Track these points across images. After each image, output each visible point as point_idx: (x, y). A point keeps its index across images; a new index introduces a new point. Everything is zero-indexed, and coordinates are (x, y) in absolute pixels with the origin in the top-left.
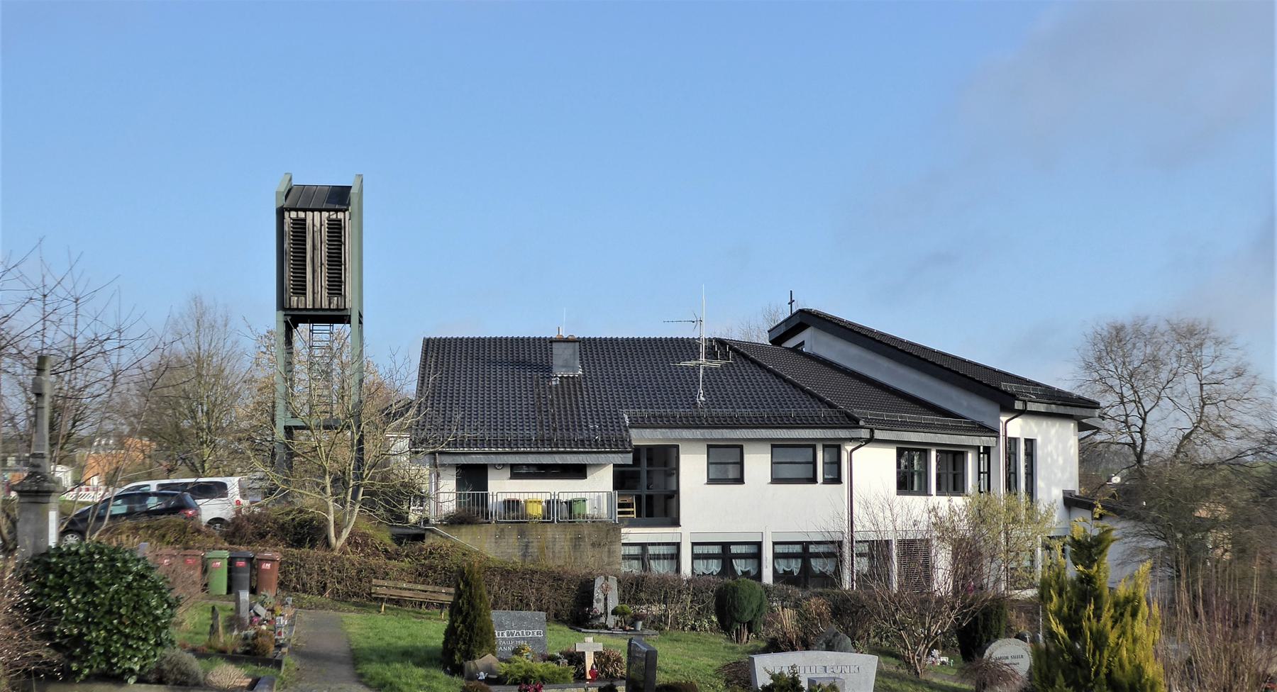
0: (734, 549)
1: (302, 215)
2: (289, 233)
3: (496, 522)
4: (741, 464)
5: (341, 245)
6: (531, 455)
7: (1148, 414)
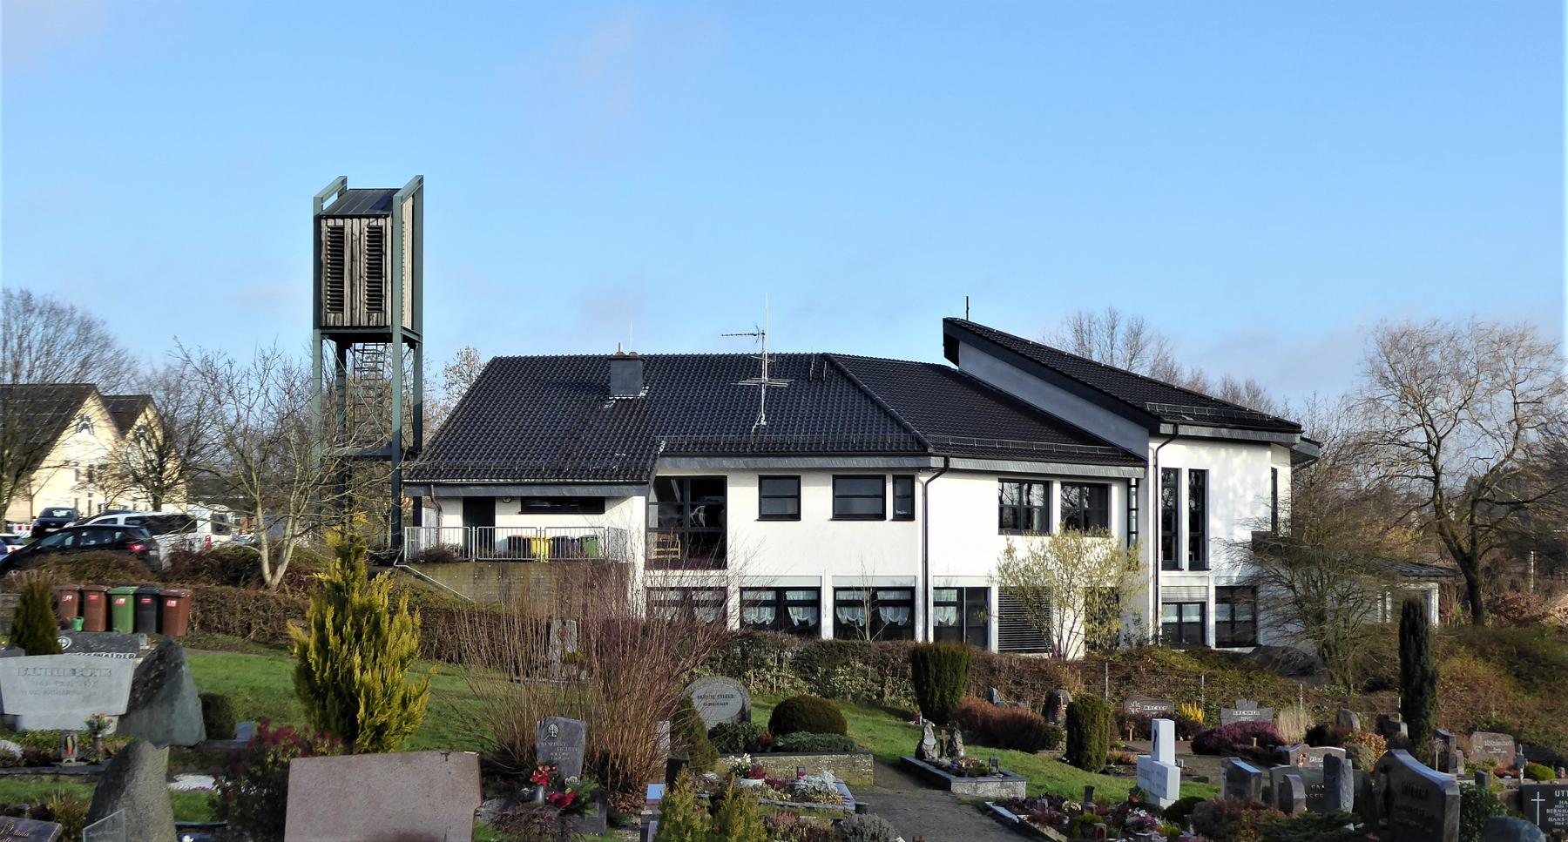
0: (790, 596)
3: (476, 560)
4: (798, 497)
5: (382, 256)
7: (1443, 441)
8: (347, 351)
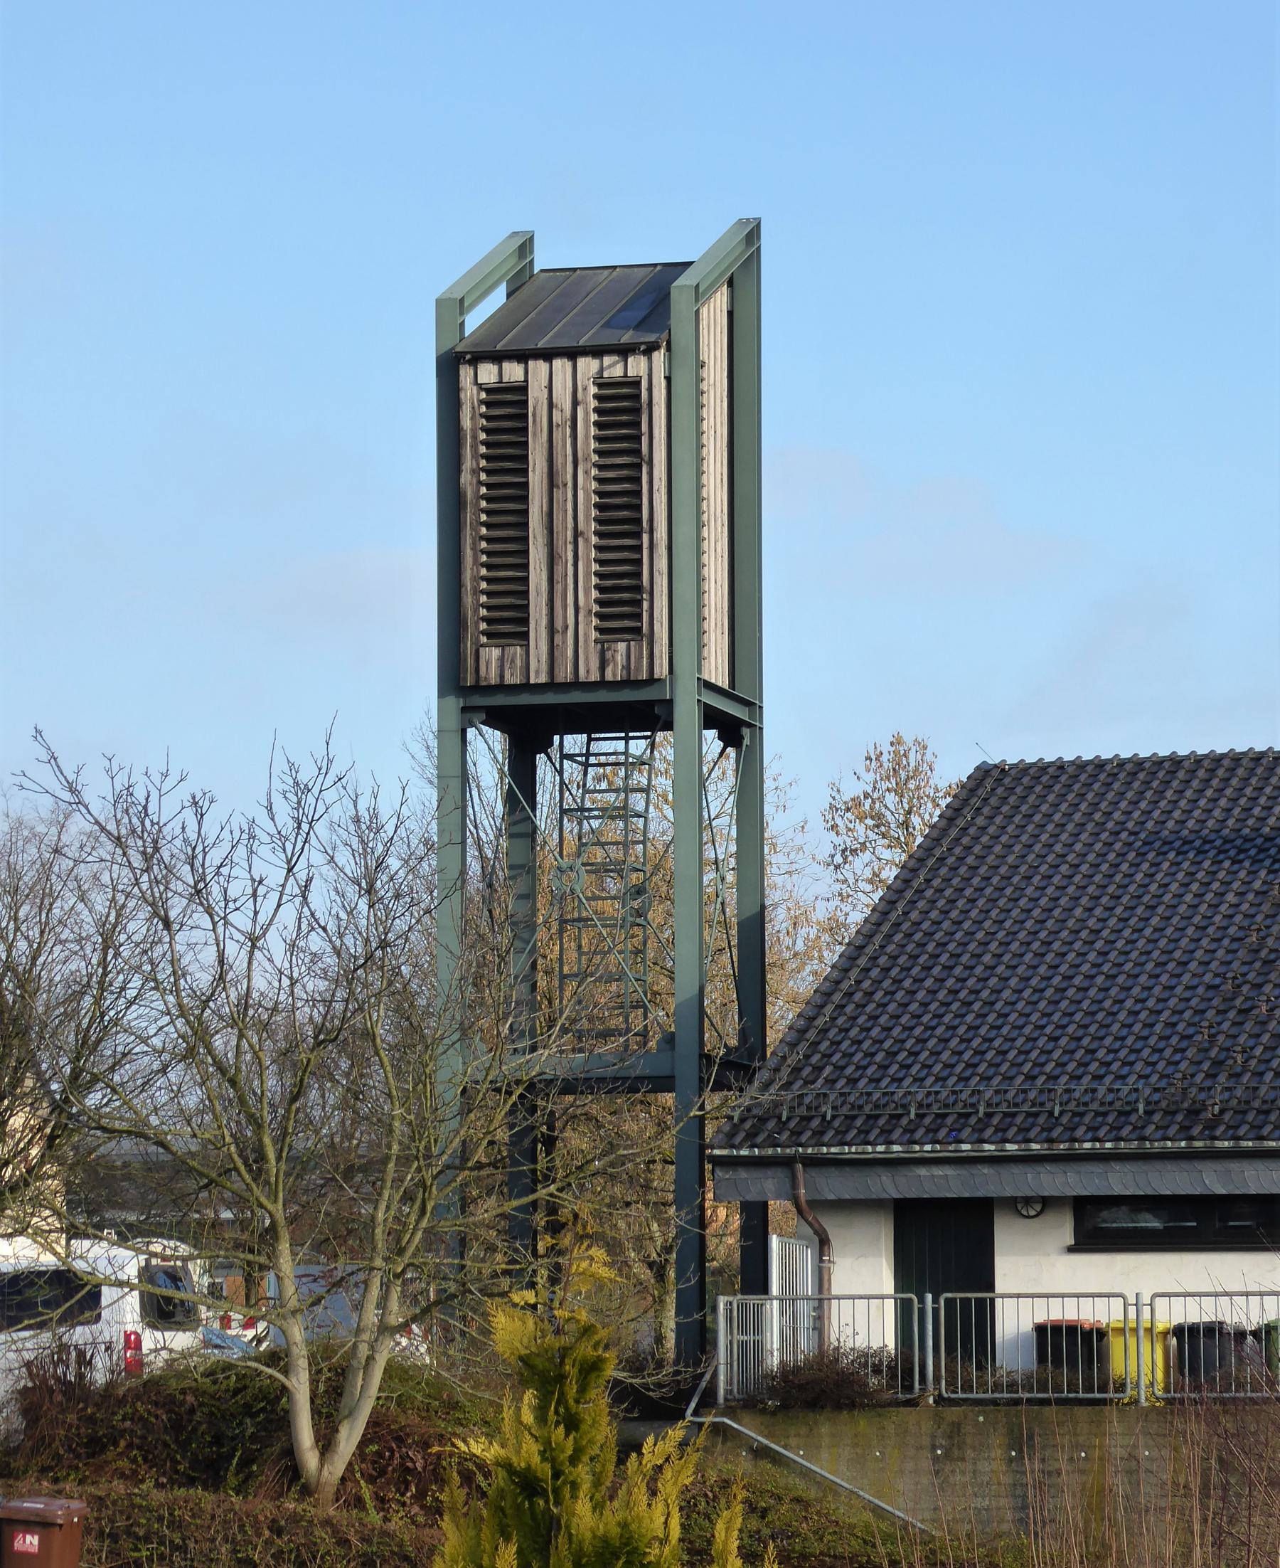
1: (514, 372)
2: (474, 437)
3: (940, 1400)
5: (639, 467)
6: (1117, 1166)
8: (541, 759)
